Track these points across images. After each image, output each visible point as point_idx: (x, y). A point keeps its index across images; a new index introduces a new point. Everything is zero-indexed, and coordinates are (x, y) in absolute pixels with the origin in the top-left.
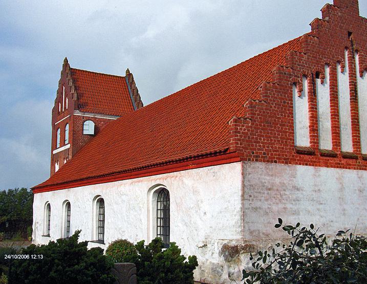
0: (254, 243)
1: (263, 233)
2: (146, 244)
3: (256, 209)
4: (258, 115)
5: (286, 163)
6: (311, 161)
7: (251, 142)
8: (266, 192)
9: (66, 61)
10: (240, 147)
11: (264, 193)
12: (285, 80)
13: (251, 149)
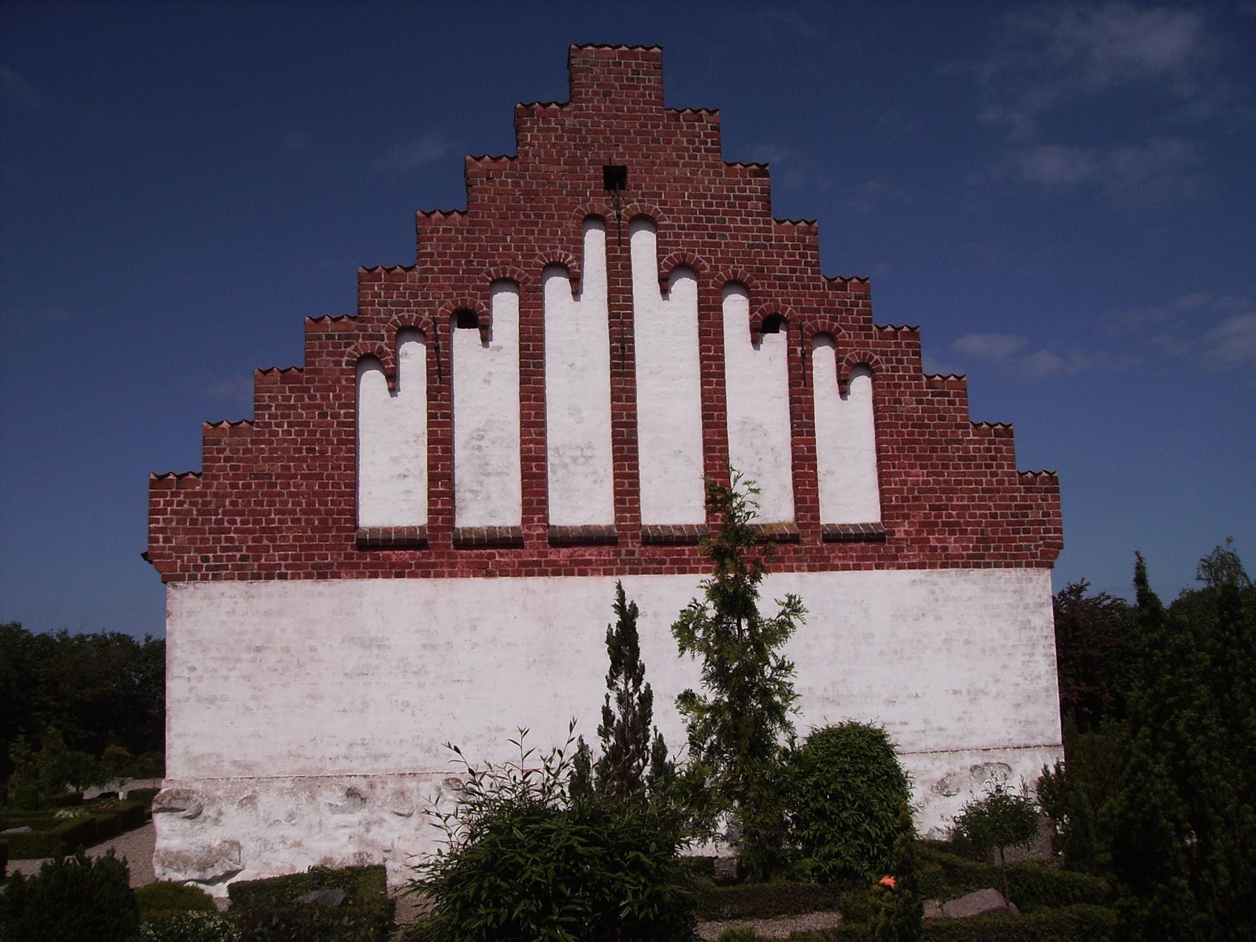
0: (198, 786)
1: (235, 763)
2: (1085, 595)
3: (212, 700)
4: (227, 459)
5: (323, 576)
6: (418, 565)
7: (202, 531)
8: (246, 656)
9: (393, 390)
10: (163, 548)
11: (238, 660)
12: (329, 354)
13: (197, 550)
